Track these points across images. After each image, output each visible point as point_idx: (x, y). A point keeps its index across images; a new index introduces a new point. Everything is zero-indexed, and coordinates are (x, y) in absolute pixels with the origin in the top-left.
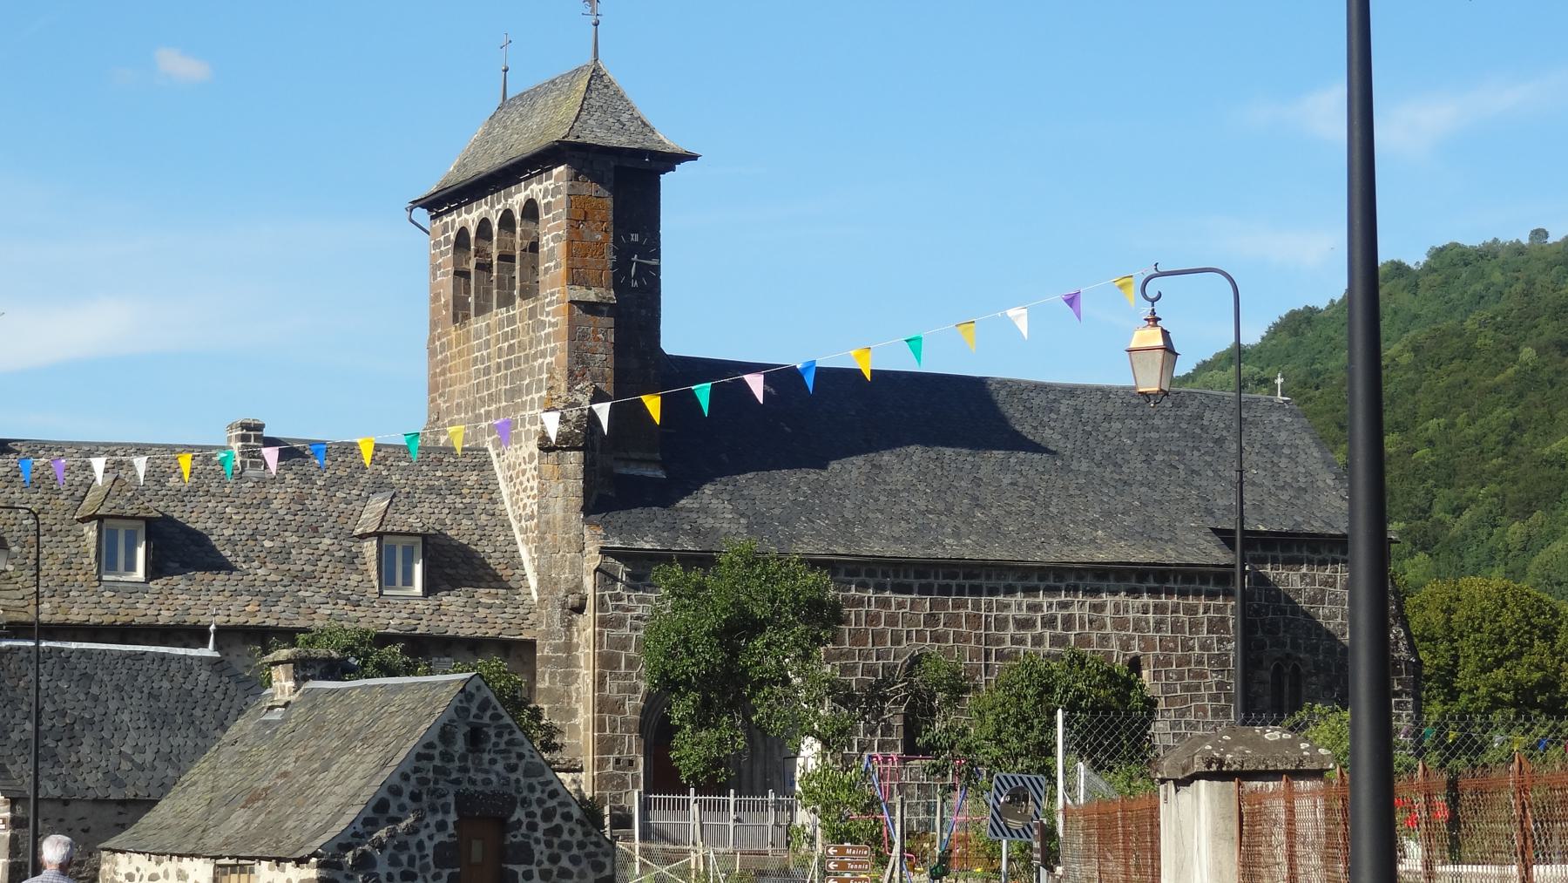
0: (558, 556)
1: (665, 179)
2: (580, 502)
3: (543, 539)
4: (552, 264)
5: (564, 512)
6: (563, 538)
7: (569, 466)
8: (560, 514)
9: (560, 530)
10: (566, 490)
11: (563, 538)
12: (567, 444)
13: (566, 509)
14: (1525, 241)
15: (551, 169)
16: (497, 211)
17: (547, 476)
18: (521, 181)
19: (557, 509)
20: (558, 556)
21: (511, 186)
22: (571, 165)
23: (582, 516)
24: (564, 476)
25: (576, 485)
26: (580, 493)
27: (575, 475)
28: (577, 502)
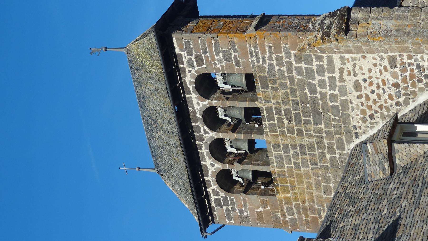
0: (422, 23)
1: (234, 178)
2: (386, 9)
3: (409, 33)
4: (233, 53)
5: (392, 19)
6: (410, 20)
7: (361, 16)
8: (393, 22)
9: (404, 22)
10: (377, 18)
11: (410, 20)
12: (344, 16)
13: (390, 18)
14: (340, 9)
15: (175, 54)
16: (206, 132)
17: (365, 30)
18: (185, 97)
19: (388, 24)
20: (422, 23)
21: (188, 112)
22: (174, 31)
23: (396, 8)
24: (367, 20)
25: (375, 12)
26: (380, 9)
27: (367, 12)
28: (386, 11)
